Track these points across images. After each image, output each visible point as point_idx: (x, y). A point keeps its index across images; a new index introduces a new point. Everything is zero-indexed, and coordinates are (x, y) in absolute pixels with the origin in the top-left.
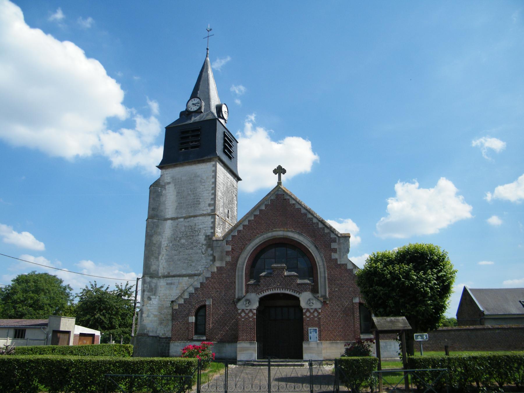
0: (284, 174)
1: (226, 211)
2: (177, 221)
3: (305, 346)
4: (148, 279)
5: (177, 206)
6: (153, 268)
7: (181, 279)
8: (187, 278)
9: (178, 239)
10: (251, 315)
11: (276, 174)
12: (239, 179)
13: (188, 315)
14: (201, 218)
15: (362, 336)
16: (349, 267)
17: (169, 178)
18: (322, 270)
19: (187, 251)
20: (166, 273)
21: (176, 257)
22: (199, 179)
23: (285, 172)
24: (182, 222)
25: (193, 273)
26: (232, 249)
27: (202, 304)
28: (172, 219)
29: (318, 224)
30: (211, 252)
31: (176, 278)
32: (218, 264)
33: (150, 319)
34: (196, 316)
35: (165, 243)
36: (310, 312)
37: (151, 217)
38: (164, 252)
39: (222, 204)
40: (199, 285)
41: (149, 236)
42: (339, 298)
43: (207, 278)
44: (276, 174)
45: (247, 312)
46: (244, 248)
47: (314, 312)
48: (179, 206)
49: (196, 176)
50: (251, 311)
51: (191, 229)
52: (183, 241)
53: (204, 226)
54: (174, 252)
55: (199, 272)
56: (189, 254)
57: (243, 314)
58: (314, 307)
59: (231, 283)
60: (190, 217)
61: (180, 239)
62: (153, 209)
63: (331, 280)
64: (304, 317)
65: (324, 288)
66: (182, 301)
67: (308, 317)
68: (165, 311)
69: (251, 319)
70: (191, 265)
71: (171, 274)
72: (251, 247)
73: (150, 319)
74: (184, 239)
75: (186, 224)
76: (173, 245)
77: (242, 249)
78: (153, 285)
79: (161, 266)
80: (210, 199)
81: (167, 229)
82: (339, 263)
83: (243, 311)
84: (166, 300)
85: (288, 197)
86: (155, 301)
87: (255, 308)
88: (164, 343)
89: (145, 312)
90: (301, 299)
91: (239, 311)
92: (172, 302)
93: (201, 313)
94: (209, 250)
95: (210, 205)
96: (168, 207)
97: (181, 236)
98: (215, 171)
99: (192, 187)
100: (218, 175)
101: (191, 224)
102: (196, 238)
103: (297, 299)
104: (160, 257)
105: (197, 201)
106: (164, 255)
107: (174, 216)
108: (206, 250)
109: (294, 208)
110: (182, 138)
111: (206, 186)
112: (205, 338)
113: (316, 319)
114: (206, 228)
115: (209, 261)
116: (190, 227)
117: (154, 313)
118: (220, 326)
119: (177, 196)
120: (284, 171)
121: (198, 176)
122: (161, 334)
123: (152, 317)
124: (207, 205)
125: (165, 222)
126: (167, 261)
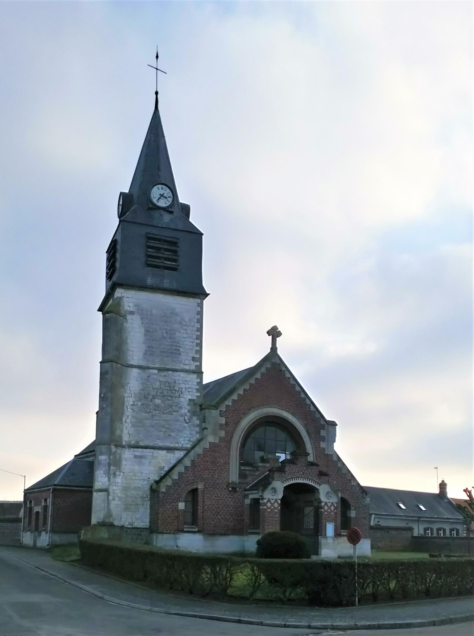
7: (155, 452)
9: (150, 397)
11: (269, 335)
14: (182, 374)
15: (342, 531)
16: (335, 459)
17: (131, 305)
19: (163, 415)
20: (133, 442)
21: (148, 422)
24: (155, 374)
25: (172, 445)
28: (139, 367)
30: (198, 422)
31: (148, 450)
35: (129, 401)
40: (190, 463)
43: (199, 455)
45: (272, 501)
48: (149, 351)
49: (174, 313)
50: (276, 501)
52: (158, 401)
53: (187, 386)
54: (144, 415)
55: (180, 445)
56: (167, 420)
58: (331, 500)
60: (168, 370)
61: (154, 397)
67: (326, 511)
69: (276, 511)
70: (170, 435)
71: (141, 444)
72: (246, 422)
74: (159, 400)
76: (142, 404)
77: (237, 423)
79: (125, 431)
80: (194, 351)
81: (133, 382)
83: (269, 500)
84: (134, 478)
90: (320, 491)
91: (323, 504)
94: (195, 418)
95: (194, 359)
96: (132, 349)
97: (153, 393)
99: (168, 328)
101: (170, 380)
102: (176, 400)
105: (176, 350)
106: (130, 417)
107: (142, 363)
108: (190, 419)
112: (196, 530)
114: (189, 390)
115: (194, 433)
116: (167, 384)
118: (213, 515)
119: (145, 335)
122: (127, 523)
124: (190, 358)
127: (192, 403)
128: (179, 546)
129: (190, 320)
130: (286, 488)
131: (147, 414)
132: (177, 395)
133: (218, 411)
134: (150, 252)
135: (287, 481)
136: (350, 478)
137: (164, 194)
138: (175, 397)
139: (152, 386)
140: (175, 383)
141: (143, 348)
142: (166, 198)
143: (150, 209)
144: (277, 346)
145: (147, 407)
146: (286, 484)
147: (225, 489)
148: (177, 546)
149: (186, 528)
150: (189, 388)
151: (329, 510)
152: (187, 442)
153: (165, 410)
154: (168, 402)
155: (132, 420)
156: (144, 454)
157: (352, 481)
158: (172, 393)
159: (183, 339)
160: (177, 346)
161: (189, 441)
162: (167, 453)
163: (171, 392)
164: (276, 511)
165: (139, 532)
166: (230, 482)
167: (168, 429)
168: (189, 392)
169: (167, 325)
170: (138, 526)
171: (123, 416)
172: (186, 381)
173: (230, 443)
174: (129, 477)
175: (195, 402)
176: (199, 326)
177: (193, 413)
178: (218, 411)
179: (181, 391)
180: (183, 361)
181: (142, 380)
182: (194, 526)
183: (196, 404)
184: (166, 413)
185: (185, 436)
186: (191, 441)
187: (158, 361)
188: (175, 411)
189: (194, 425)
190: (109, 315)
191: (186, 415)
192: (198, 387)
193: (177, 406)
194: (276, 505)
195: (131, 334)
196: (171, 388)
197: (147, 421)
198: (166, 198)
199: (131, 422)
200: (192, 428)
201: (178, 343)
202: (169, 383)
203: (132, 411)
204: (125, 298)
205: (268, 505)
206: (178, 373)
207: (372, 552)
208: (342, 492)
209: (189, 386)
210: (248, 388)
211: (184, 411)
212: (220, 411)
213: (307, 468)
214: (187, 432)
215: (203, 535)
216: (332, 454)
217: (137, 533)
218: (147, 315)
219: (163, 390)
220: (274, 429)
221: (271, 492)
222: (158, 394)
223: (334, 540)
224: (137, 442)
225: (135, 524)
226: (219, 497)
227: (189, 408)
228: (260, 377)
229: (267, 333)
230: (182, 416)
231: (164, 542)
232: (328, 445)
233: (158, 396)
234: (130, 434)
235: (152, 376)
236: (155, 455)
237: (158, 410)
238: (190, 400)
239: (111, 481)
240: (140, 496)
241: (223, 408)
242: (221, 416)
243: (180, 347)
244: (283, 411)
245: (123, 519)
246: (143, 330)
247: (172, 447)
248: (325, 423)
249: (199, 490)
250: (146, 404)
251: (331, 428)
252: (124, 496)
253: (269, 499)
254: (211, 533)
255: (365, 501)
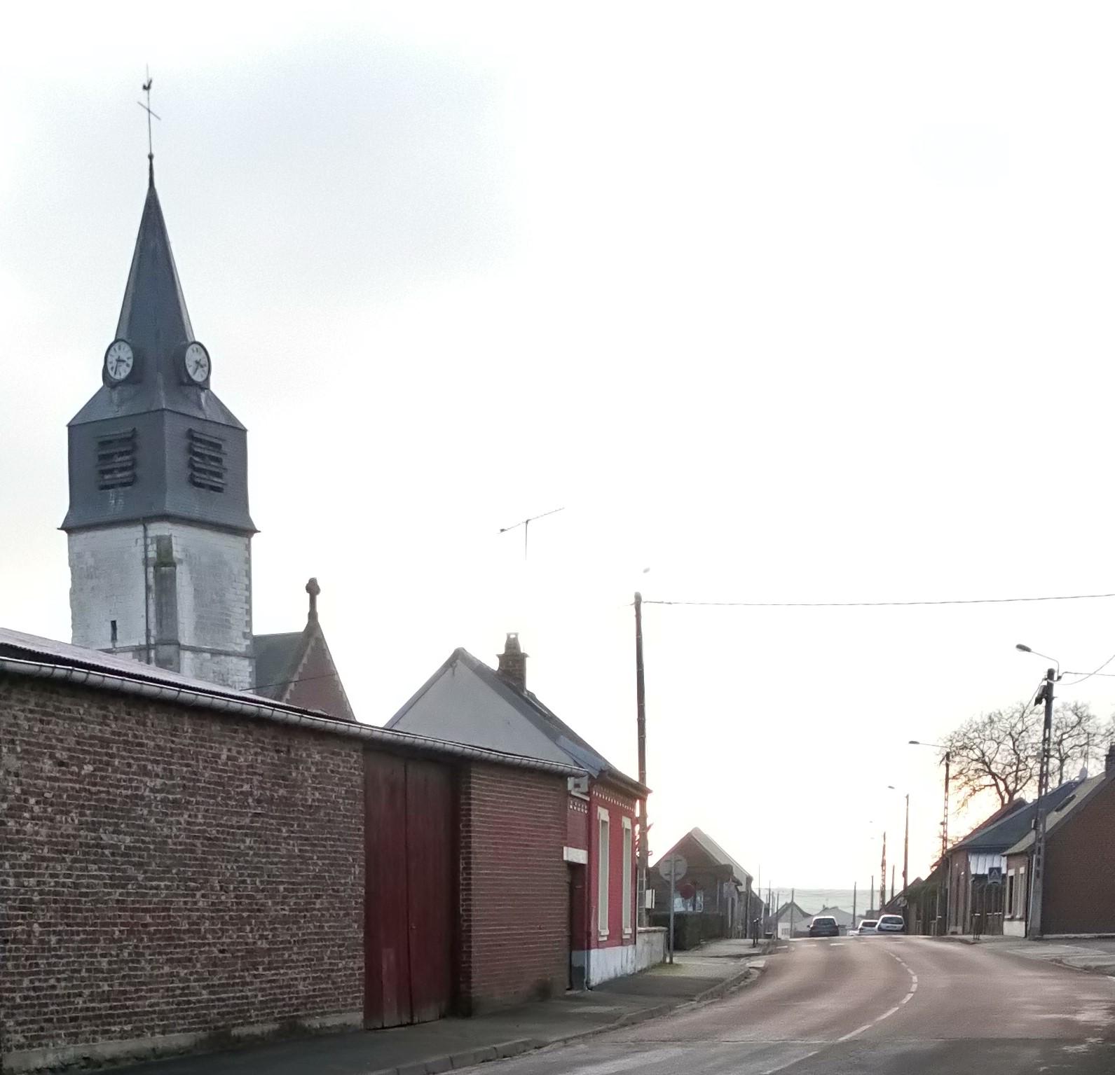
14: (234, 660)
24: (208, 660)
134: (213, 466)
143: (182, 383)
150: (242, 682)
176: (248, 583)
190: (167, 568)
195: (181, 595)
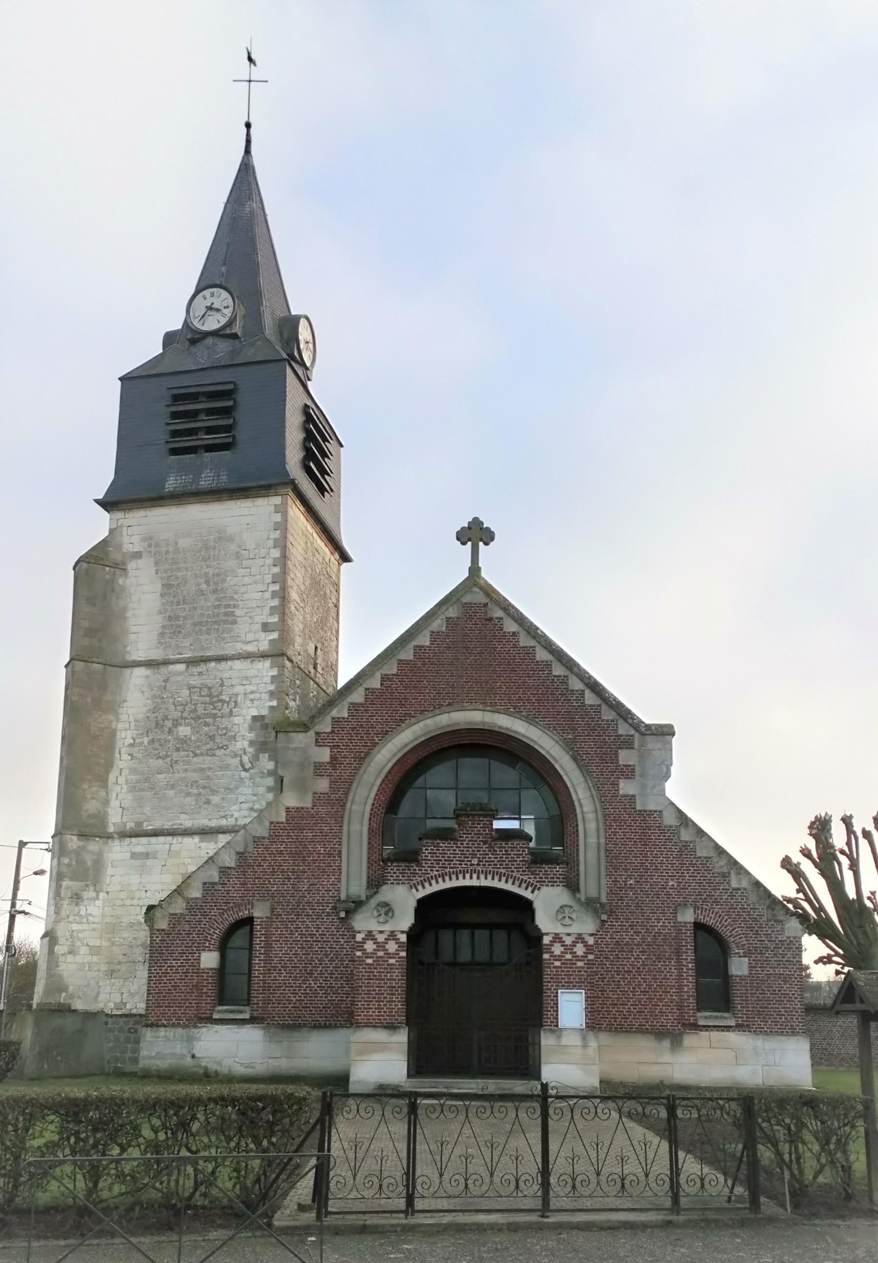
0: (486, 544)
1: (311, 650)
2: (163, 670)
3: (547, 1040)
4: (73, 842)
5: (164, 627)
6: (91, 806)
7: (175, 840)
8: (197, 839)
9: (169, 724)
10: (392, 947)
11: (464, 543)
12: (345, 558)
13: (202, 948)
14: (238, 665)
15: (699, 1014)
16: (669, 819)
17: (136, 539)
18: (592, 826)
20: (130, 825)
22: (233, 547)
23: (492, 539)
24: (180, 673)
25: (214, 823)
26: (333, 758)
27: (244, 914)
28: (150, 664)
29: (582, 692)
30: (271, 765)
31: (161, 839)
32: (291, 800)
33: (79, 959)
34: (223, 947)
35: (125, 736)
36: (562, 942)
37: (79, 657)
38: (123, 761)
39: (301, 626)
40: (234, 857)
41: (74, 712)
42: (637, 906)
43: (257, 840)
44: (464, 543)
45: (381, 938)
46: (367, 754)
47: (574, 943)
48: (172, 628)
49: (223, 538)
50: (392, 936)
51: (210, 696)
52: (184, 731)
53: (249, 688)
55: (231, 822)
56: (203, 770)
57: (370, 946)
58: (575, 929)
59: (330, 855)
60: (206, 660)
61: (176, 723)
62: (91, 632)
63: (613, 859)
64: (546, 956)
65: (593, 877)
66: (179, 907)
68: (125, 935)
69: (392, 961)
70: (208, 802)
71: (147, 827)
72: (387, 754)
73: (79, 959)
75: (195, 681)
76: (152, 742)
77: (362, 758)
78: (89, 859)
79: (114, 803)
80: (267, 610)
81: (136, 694)
82: (638, 808)
83: (370, 935)
84: (128, 902)
85: (499, 613)
86: (95, 909)
87: (406, 929)
88: (121, 1030)
89: (61, 940)
90: (537, 905)
91: (359, 937)
92: (150, 908)
93: (239, 939)
94: (264, 758)
95: (266, 627)
97: (176, 714)
98: (283, 527)
100: (290, 538)
101: (209, 682)
102: (225, 722)
103: (527, 907)
104: (112, 778)
105: (226, 614)
106: (125, 772)
107: (156, 654)
108: (256, 758)
109: (515, 646)
110: (227, 412)
111: (254, 571)
113: (580, 964)
114: (252, 696)
115: (262, 790)
116: (205, 692)
117: (92, 943)
119: (162, 596)
120: (488, 536)
121: (231, 539)
122: (112, 1005)
123: (83, 956)
124: (259, 627)
125: (127, 671)
126: (132, 789)
127: (258, 724)
128: (197, 1055)
129: (258, 546)
130: (420, 902)
131: (161, 761)
132: (226, 710)
133: (311, 734)
135: (427, 884)
136: (725, 870)
137: (213, 304)
138: (222, 717)
139: (171, 700)
140: (222, 685)
141: (158, 621)
142: (218, 310)
144: (480, 565)
145: (161, 745)
146: (422, 893)
147: (328, 915)
148: (193, 1056)
149: (219, 1012)
150: (252, 692)
151: (569, 956)
152: (246, 813)
153: (198, 747)
154: (207, 729)
155: (130, 777)
156: (151, 849)
157: (733, 876)
158: (215, 708)
159: (243, 589)
160: (228, 606)
161: (251, 809)
162: (200, 842)
163: (214, 704)
164: (392, 961)
165: (131, 1025)
166: (343, 897)
167: (204, 788)
168: (252, 700)
169: (208, 566)
170: (134, 1011)
171: (108, 772)
172: (247, 678)
173: (344, 806)
174: (118, 902)
175: (266, 721)
177: (261, 747)
178: (311, 734)
179: (236, 702)
180: (243, 636)
181: (152, 690)
182: (726, 1015)
183: (267, 724)
184: (202, 754)
185: (242, 799)
186: (255, 811)
187: (188, 644)
188: (222, 748)
189: (263, 773)
191: (245, 753)
192: (272, 688)
193: (225, 734)
194: (392, 947)
196: (214, 697)
197: (159, 776)
198: (218, 310)
199: (127, 781)
200: (258, 780)
201: (232, 598)
202: (210, 688)
203: (130, 757)
204: (125, 529)
205: (366, 946)
206: (230, 663)
207: (814, 1071)
208: (696, 908)
209: (254, 688)
210: (395, 672)
211: (242, 744)
212: (317, 733)
213: (490, 847)
214: (246, 791)
215: (264, 1028)
216: (659, 809)
217: (126, 1028)
218: (167, 552)
219: (195, 705)
220: (486, 761)
221: (375, 913)
222: (185, 715)
223: (584, 1038)
224: (139, 824)
225: (128, 1006)
226: (312, 936)
227: (251, 736)
228: (428, 644)
229: (458, 539)
230: (236, 756)
231: (161, 1048)
232: (643, 787)
233: (185, 719)
234: (123, 808)
235: (172, 679)
236: (174, 848)
237: (184, 750)
238: (255, 718)
239: (63, 914)
240: (139, 943)
241: (325, 726)
242: (318, 744)
243: (235, 606)
244: (497, 715)
245: (102, 997)
246: (158, 587)
247: (211, 828)
248: (632, 732)
249: (257, 922)
250: (159, 740)
251: (651, 743)
252: (108, 944)
253: (370, 932)
254: (287, 1023)
255: (783, 930)
